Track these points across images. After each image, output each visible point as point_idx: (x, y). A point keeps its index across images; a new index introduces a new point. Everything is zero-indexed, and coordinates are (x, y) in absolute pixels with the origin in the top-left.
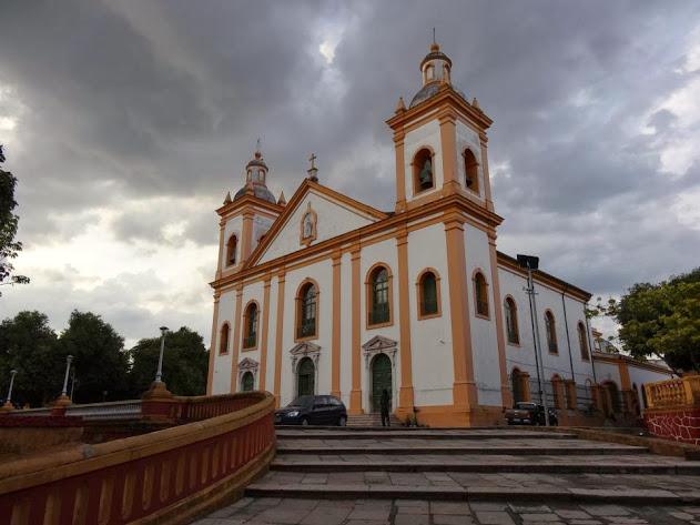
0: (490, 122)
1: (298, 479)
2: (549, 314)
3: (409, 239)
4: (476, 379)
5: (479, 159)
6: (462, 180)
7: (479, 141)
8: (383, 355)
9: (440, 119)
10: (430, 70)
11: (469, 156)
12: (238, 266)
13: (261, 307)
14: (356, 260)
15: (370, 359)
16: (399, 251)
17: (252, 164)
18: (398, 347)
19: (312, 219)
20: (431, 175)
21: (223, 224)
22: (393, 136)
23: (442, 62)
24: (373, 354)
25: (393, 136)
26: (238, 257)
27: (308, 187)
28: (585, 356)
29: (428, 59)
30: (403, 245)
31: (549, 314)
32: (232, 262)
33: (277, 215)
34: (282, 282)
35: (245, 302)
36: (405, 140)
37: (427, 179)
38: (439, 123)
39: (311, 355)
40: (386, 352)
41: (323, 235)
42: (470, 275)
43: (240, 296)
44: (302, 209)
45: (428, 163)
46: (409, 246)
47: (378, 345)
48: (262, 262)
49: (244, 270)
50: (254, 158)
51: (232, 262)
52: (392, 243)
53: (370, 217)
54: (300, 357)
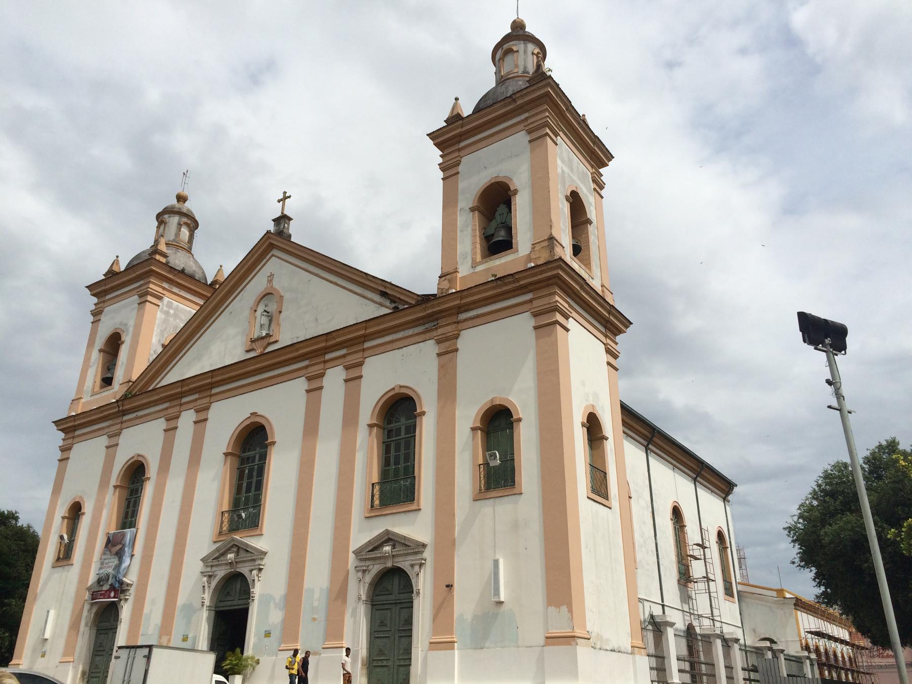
0: (610, 157)
1: (364, 597)
2: (677, 513)
3: (460, 343)
4: (589, 627)
5: (591, 213)
6: (565, 239)
7: (593, 186)
8: (241, 576)
9: (529, 132)
10: (509, 59)
11: (576, 202)
12: (117, 389)
13: (152, 471)
14: (353, 380)
15: (368, 578)
16: (441, 367)
17: (169, 211)
18: (428, 554)
19: (272, 308)
20: (509, 230)
21: (97, 313)
22: (440, 160)
23: (531, 47)
24: (376, 568)
25: (440, 160)
26: (119, 375)
27: (272, 246)
28: (728, 591)
29: (507, 39)
30: (448, 352)
31: (677, 513)
32: (107, 381)
33: (201, 302)
34: (201, 422)
35: (122, 459)
36: (460, 168)
37: (501, 235)
38: (528, 138)
39: (244, 570)
40: (404, 564)
41: (286, 336)
42: (578, 418)
43: (112, 447)
44: (257, 285)
45: (502, 209)
46: (461, 357)
47: (387, 548)
48: (163, 383)
49: (125, 398)
50: (173, 201)
51: (107, 381)
52: (429, 349)
53: (388, 303)
54: (221, 573)
